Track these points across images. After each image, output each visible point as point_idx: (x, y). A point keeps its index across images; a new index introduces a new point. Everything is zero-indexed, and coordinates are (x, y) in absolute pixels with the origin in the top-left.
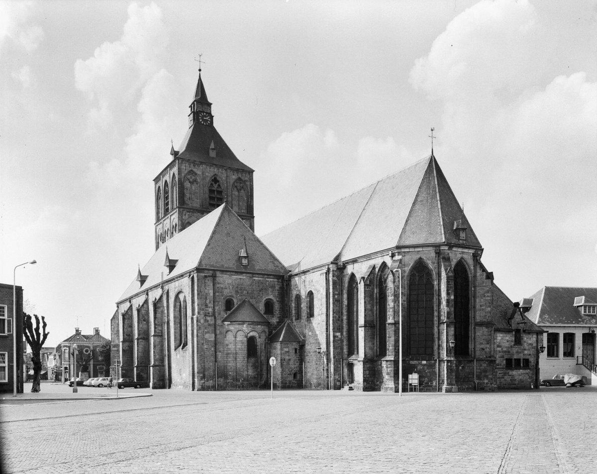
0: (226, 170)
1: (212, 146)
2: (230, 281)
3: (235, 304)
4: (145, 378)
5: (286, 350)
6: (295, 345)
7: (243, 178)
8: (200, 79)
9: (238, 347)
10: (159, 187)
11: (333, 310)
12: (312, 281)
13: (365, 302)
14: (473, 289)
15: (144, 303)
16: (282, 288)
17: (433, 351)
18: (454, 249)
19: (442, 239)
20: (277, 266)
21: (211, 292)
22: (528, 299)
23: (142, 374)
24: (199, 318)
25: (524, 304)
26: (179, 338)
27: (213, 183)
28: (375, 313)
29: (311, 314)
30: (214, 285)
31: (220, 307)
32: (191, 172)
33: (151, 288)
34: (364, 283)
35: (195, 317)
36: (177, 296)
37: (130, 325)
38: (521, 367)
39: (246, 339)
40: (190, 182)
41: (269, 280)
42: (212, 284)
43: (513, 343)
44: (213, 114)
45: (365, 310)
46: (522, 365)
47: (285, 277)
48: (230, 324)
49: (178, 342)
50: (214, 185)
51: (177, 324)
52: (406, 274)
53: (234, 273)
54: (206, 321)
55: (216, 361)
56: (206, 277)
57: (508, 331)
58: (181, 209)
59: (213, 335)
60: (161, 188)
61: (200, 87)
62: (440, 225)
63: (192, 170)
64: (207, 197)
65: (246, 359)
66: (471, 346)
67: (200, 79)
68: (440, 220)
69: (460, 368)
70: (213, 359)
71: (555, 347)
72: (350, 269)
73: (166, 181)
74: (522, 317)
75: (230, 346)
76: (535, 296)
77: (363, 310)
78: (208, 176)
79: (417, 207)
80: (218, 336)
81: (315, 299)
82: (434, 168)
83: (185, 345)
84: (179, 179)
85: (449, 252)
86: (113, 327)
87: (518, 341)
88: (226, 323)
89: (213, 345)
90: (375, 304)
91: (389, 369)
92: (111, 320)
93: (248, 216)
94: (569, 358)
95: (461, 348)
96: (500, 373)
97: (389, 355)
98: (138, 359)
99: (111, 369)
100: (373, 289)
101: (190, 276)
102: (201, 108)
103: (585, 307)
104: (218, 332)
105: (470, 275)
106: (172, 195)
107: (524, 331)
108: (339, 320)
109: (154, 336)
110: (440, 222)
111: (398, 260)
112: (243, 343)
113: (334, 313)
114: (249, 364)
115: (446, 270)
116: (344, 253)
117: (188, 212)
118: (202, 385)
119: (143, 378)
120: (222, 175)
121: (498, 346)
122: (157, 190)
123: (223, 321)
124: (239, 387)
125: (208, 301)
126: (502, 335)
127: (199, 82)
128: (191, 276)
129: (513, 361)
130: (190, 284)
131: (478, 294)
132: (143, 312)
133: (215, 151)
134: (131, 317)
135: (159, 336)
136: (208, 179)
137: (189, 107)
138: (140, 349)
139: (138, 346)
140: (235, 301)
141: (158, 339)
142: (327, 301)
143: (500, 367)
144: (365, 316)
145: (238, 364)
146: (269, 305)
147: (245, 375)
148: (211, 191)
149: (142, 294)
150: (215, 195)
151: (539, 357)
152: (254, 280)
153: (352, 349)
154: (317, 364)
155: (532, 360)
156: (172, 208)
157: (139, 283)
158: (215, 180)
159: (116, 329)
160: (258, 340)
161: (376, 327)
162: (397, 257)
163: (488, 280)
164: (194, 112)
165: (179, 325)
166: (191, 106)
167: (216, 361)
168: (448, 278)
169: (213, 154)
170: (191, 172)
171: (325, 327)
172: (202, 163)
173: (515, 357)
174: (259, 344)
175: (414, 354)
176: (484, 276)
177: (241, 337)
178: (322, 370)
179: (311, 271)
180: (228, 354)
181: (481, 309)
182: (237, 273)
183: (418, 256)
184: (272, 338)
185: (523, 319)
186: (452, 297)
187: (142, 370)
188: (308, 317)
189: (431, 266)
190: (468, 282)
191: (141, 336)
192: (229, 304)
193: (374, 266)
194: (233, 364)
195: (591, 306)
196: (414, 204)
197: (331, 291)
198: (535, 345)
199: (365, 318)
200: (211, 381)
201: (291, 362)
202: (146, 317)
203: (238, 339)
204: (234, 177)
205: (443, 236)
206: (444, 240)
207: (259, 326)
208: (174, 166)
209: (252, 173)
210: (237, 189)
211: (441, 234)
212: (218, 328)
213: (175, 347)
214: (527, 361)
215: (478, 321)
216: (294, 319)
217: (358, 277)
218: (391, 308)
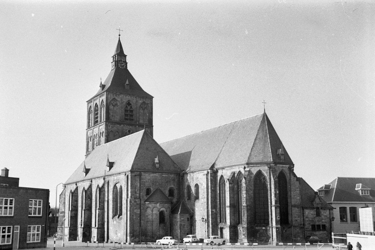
0: (136, 97)
1: (127, 83)
2: (149, 178)
3: (152, 191)
5: (183, 219)
6: (187, 216)
7: (146, 102)
8: (119, 41)
9: (154, 217)
11: (211, 196)
12: (198, 178)
13: (230, 193)
14: (289, 186)
16: (179, 181)
17: (268, 222)
18: (278, 165)
19: (271, 160)
20: (176, 168)
21: (139, 184)
22: (328, 185)
23: (86, 233)
24: (131, 200)
25: (325, 188)
26: (115, 211)
27: (128, 105)
28: (235, 199)
29: (197, 198)
30: (140, 180)
31: (143, 193)
34: (229, 182)
35: (129, 199)
36: (115, 186)
37: (76, 200)
38: (321, 230)
39: (158, 212)
40: (113, 105)
41: (171, 176)
42: (139, 180)
43: (315, 216)
44: (127, 61)
45: (230, 198)
46: (321, 228)
47: (181, 174)
49: (114, 213)
50: (128, 107)
52: (252, 179)
53: (151, 173)
54: (135, 202)
55: (140, 226)
56: (135, 175)
57: (313, 208)
58: (107, 123)
59: (139, 210)
61: (120, 46)
62: (270, 152)
63: (114, 98)
65: (158, 225)
66: (290, 219)
67: (119, 41)
68: (269, 149)
69: (284, 231)
70: (139, 225)
71: (345, 216)
72: (219, 174)
73: (96, 103)
74: (320, 200)
76: (332, 183)
77: (229, 200)
78: (124, 102)
79: (257, 141)
80: (142, 211)
81: (199, 189)
82: (265, 119)
83: (121, 214)
84: (106, 104)
85: (275, 167)
87: (318, 214)
88: (147, 203)
89: (139, 216)
90: (235, 194)
91: (244, 232)
92: (60, 195)
93: (150, 126)
94: (354, 223)
95: (284, 220)
96: (308, 234)
97: (244, 224)
99: (58, 229)
100: (234, 186)
101: (126, 174)
102: (120, 58)
103: (362, 190)
104: (142, 208)
105: (287, 179)
107: (321, 208)
108: (214, 202)
110: (270, 151)
111: (247, 171)
112: (156, 215)
113: (211, 198)
114: (160, 228)
115: (274, 177)
116: (217, 163)
117: (111, 124)
120: (133, 100)
121: (307, 218)
122: (89, 109)
123: (145, 201)
125: (136, 190)
126: (308, 211)
127: (118, 43)
128: (127, 175)
129: (316, 226)
130: (126, 180)
131: (292, 190)
132: (88, 193)
133: (129, 86)
135: (102, 209)
136: (124, 103)
138: (86, 216)
139: (84, 215)
140: (152, 189)
142: (207, 191)
143: (308, 230)
144: (230, 201)
146: (171, 192)
148: (126, 111)
150: (129, 113)
152: (163, 176)
153: (223, 219)
154: (201, 228)
155: (327, 225)
156: (101, 121)
157: (85, 174)
158: (129, 104)
159: (63, 201)
160: (166, 213)
161: (235, 207)
162: (247, 169)
163: (297, 182)
164: (115, 61)
165: (115, 203)
166: (113, 57)
167: (140, 226)
168: (275, 182)
169: (127, 87)
171: (206, 206)
173: (317, 223)
174: (166, 215)
175: (258, 223)
176: (295, 180)
177: (156, 212)
178: (205, 232)
179: (197, 172)
180: (147, 221)
181: (295, 197)
182: (154, 172)
183: (258, 169)
184: (174, 211)
185: (321, 201)
186: (278, 192)
188: (195, 199)
189: (265, 174)
190: (287, 182)
192: (148, 191)
193: (234, 172)
195: (368, 190)
196: (255, 140)
197: (210, 185)
198: (328, 216)
199: (230, 202)
200: (137, 238)
201: (186, 226)
202: (90, 196)
203: (154, 212)
204: (140, 101)
205: (272, 158)
206: (272, 160)
207: (166, 205)
208: (103, 95)
209: (152, 99)
210: (143, 109)
211: (271, 157)
212: (142, 205)
214: (324, 226)
215: (293, 204)
217: (225, 177)
218: (244, 198)
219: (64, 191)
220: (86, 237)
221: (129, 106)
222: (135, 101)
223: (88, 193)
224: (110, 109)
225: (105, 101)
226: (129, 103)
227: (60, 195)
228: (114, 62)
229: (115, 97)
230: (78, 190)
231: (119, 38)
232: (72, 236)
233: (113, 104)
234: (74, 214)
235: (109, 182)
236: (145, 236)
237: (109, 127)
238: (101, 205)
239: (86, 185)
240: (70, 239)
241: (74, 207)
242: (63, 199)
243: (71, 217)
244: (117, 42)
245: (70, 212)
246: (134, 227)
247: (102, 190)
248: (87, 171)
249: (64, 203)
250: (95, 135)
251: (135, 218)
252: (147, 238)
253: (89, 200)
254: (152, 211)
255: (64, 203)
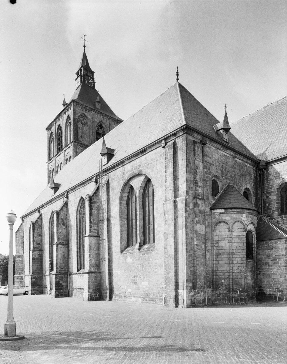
0: (109, 119)
4: (65, 287)
9: (234, 244)
10: (52, 133)
15: (64, 206)
23: (61, 282)
24: (188, 200)
26: (125, 237)
32: (83, 115)
33: (75, 188)
37: (39, 234)
40: (82, 123)
48: (224, 213)
49: (125, 242)
50: (100, 129)
51: (124, 220)
60: (54, 133)
61: (85, 58)
64: (95, 137)
65: (245, 262)
73: (60, 125)
75: (222, 244)
78: (96, 121)
86: (17, 239)
88: (217, 211)
92: (16, 233)
98: (57, 265)
102: (86, 74)
106: (66, 134)
109: (90, 236)
112: (241, 239)
117: (81, 146)
118: (191, 299)
119: (62, 286)
122: (49, 137)
123: (211, 209)
124: (236, 301)
132: (62, 215)
134: (41, 226)
136: (96, 124)
137: (76, 74)
139: (57, 252)
141: (94, 240)
145: (235, 268)
147: (243, 283)
149: (58, 199)
151: (175, 272)
159: (21, 241)
164: (81, 75)
165: (126, 222)
166: (77, 73)
170: (83, 115)
172: (92, 109)
177: (238, 232)
180: (218, 254)
187: (61, 278)
191: (60, 241)
194: (228, 268)
213: (121, 249)
216: (276, 214)
219: (22, 226)
220: (61, 289)
221: (101, 129)
222: (108, 124)
223: (62, 217)
224: (79, 127)
225: (72, 117)
226: (101, 124)
227: (16, 232)
228: (80, 77)
229: (84, 112)
230: (42, 218)
231: (84, 49)
232: (36, 288)
233: (82, 122)
234: (38, 255)
235: (110, 181)
236: (213, 288)
237: (78, 149)
238: (94, 229)
239: (57, 205)
240: (33, 292)
241: (37, 244)
242: (20, 238)
243: (33, 259)
244: (82, 55)
245: (31, 252)
246: (194, 266)
247: (95, 199)
248: (56, 187)
249: (23, 243)
250: (58, 165)
251: (197, 245)
252: (218, 292)
253: (64, 227)
254: (230, 230)
255: (22, 242)
